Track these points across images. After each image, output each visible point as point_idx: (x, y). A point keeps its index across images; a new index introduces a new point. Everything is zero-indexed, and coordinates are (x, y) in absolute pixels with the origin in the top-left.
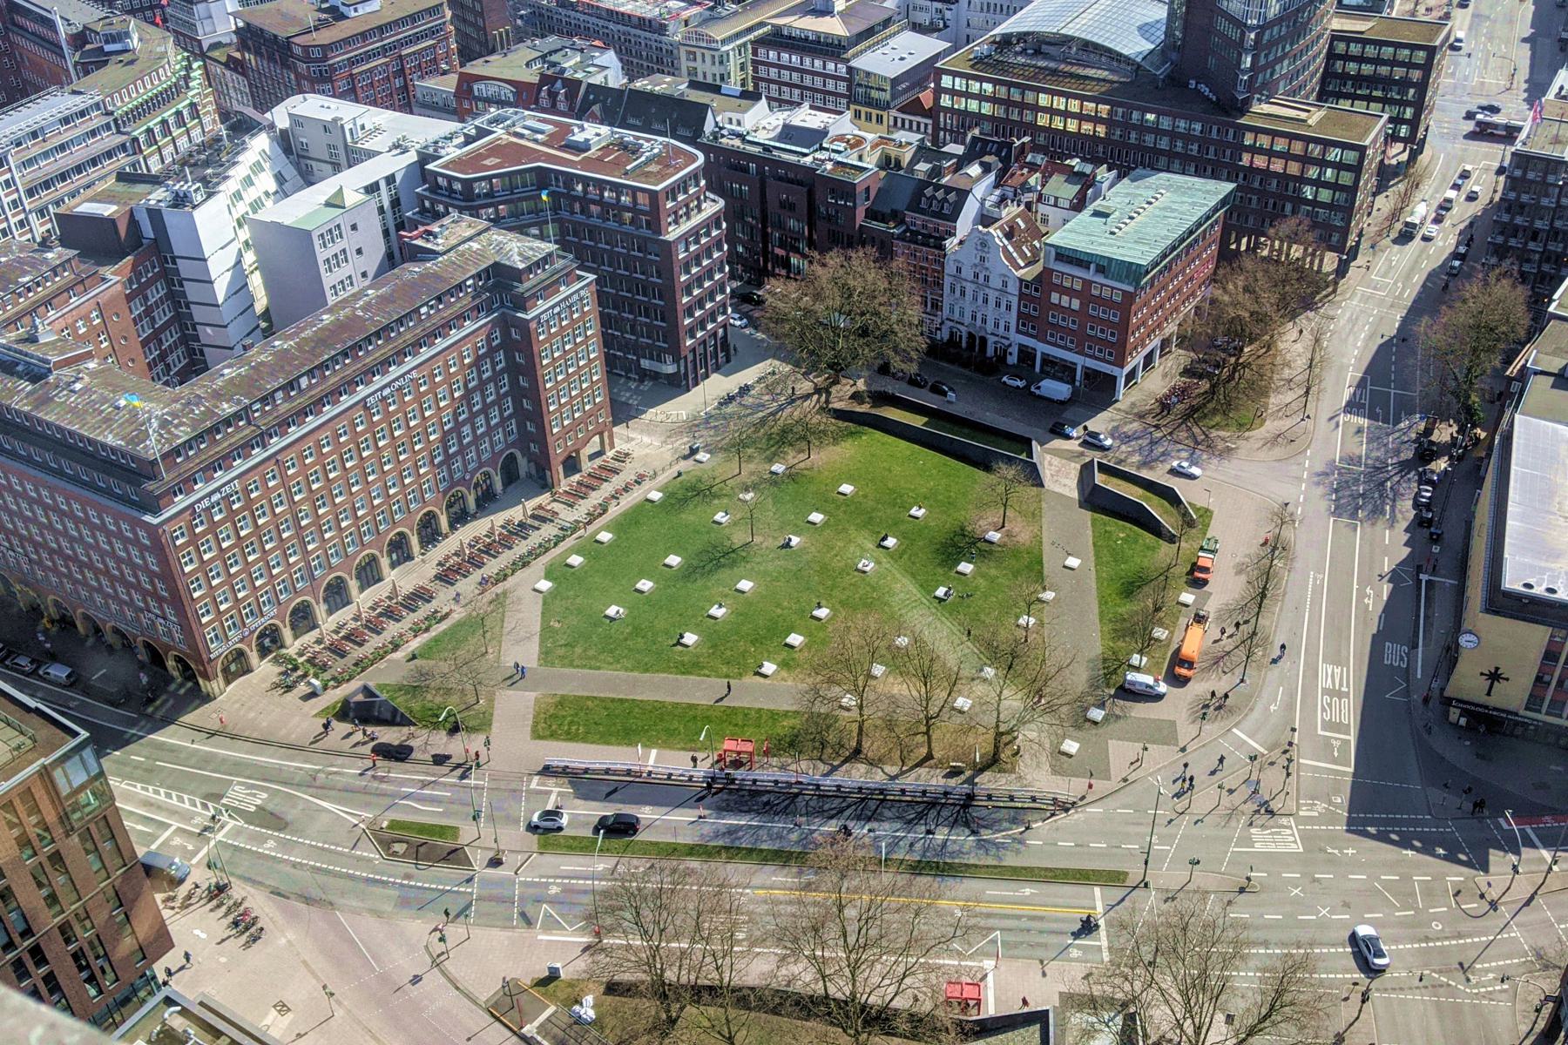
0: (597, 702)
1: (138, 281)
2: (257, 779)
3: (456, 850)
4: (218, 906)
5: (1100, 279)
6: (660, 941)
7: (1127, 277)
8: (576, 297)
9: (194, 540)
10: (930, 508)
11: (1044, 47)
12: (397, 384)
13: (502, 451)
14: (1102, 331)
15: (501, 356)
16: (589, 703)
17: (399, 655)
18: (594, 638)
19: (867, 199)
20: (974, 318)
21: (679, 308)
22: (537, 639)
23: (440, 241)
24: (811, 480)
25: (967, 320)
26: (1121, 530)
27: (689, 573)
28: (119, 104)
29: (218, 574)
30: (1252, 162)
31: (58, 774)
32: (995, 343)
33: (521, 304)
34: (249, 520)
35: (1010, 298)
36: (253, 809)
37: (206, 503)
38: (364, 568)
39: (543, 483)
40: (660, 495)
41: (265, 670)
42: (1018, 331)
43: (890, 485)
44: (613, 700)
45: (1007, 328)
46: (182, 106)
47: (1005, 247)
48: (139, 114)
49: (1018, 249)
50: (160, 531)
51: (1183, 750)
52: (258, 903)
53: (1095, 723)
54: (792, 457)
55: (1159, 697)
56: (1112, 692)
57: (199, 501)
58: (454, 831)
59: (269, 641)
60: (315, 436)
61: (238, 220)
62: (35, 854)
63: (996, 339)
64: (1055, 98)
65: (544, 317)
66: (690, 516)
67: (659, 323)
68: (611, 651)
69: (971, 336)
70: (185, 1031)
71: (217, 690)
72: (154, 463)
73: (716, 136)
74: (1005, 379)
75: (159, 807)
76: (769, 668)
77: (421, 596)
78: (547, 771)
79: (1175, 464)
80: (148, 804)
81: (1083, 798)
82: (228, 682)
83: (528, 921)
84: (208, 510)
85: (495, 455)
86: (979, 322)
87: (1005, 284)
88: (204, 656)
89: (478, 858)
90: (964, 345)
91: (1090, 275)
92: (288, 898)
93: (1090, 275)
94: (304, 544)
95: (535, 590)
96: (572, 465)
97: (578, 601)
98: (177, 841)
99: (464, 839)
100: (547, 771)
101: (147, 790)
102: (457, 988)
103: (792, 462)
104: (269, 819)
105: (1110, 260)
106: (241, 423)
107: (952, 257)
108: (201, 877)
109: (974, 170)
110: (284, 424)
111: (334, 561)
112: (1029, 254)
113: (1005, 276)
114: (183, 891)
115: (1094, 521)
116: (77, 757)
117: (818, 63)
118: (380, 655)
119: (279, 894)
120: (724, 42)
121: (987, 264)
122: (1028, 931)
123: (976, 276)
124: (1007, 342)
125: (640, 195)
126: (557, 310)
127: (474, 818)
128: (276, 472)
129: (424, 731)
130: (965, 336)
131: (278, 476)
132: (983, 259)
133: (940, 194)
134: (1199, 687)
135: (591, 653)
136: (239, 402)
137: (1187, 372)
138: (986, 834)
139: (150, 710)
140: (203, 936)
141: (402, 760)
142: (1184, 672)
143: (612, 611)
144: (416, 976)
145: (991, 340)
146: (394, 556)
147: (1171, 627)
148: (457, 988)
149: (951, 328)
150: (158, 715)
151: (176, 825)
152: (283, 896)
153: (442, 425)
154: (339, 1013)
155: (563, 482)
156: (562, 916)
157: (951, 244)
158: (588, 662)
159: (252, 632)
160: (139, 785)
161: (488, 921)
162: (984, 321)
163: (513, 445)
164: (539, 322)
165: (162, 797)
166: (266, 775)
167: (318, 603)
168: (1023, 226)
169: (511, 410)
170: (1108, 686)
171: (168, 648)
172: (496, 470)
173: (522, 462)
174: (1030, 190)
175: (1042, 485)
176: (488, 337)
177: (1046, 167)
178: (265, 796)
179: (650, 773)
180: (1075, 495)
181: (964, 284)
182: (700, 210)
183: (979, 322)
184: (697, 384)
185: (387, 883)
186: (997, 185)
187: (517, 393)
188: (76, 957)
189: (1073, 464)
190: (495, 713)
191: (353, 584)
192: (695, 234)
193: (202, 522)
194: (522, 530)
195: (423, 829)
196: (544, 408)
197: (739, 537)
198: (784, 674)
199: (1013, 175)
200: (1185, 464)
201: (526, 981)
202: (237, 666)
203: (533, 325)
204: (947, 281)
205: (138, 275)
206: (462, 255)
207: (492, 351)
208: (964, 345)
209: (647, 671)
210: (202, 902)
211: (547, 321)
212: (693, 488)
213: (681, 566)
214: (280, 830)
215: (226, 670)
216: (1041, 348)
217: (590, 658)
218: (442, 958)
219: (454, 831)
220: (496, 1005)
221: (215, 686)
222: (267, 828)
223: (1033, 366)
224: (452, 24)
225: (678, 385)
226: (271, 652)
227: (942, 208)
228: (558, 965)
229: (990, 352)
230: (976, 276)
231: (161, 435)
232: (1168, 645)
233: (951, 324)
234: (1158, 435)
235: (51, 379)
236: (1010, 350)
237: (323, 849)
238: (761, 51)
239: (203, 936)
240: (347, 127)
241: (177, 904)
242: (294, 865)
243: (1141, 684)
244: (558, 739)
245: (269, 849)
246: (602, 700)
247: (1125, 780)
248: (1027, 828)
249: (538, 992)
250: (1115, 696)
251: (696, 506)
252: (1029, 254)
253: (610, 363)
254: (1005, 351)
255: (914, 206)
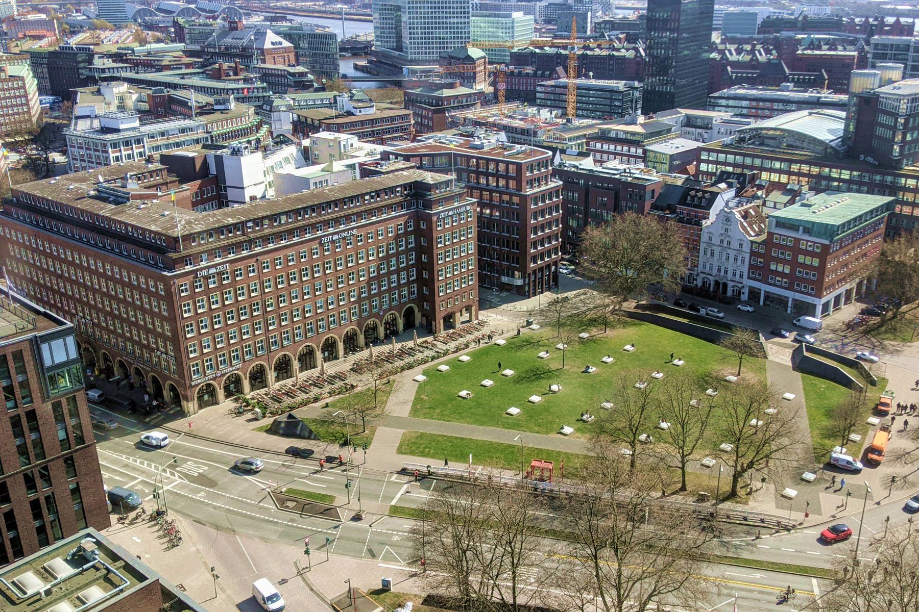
0: (445, 438)
1: (202, 196)
2: (208, 460)
3: (331, 509)
4: (155, 525)
5: (806, 237)
6: (469, 542)
7: (825, 234)
8: (464, 209)
9: (193, 296)
10: (686, 362)
11: (766, 140)
12: (343, 234)
13: (405, 303)
14: (807, 273)
15: (412, 239)
16: (440, 438)
17: (318, 404)
18: (449, 406)
19: (653, 197)
20: (719, 270)
21: (528, 240)
22: (411, 404)
23: (384, 167)
24: (606, 343)
25: (715, 272)
26: (822, 384)
27: (518, 380)
28: (215, 129)
29: (206, 326)
30: (901, 210)
31: (45, 347)
32: (733, 287)
33: (429, 205)
34: (232, 294)
35: (744, 255)
36: (196, 474)
37: (204, 273)
38: (304, 355)
39: (429, 330)
40: (505, 342)
41: (227, 404)
42: (749, 278)
43: (660, 349)
44: (456, 438)
45: (741, 276)
46: (252, 138)
47: (741, 223)
48: (226, 137)
49: (750, 225)
50: (172, 282)
51: (878, 503)
52: (183, 526)
53: (809, 482)
54: (594, 331)
55: (857, 471)
56: (822, 466)
57: (201, 269)
58: (332, 498)
59: (233, 387)
60: (285, 252)
61: (269, 183)
62: (16, 406)
63: (734, 284)
64: (772, 174)
65: (442, 216)
66: (523, 354)
67: (515, 265)
68: (460, 413)
69: (717, 283)
70: (93, 552)
71: (191, 410)
72: (176, 239)
73: (560, 165)
74: (739, 306)
75: (134, 469)
76: (568, 430)
77: (340, 377)
78: (404, 472)
79: (859, 353)
80: (126, 466)
81: (801, 524)
82: (201, 407)
83: (373, 555)
84: (206, 278)
85: (401, 305)
86: (722, 273)
87: (741, 245)
88: (187, 382)
89: (345, 516)
90: (712, 289)
91: (799, 235)
92: (205, 525)
93: (799, 235)
94: (267, 325)
95: (414, 380)
96: (449, 321)
97: (442, 387)
98: (140, 487)
99: (336, 503)
100: (404, 472)
101: (129, 459)
102: (312, 590)
103: (593, 333)
104: (203, 480)
105: (813, 223)
106: (238, 233)
107: (706, 231)
108: (150, 507)
109: (723, 186)
110: (266, 239)
111: (285, 343)
112: (757, 229)
113: (741, 240)
114: (132, 515)
115: (803, 379)
116: (61, 340)
117: (626, 148)
118: (304, 403)
119: (199, 522)
120: (570, 139)
121: (729, 233)
122: (759, 600)
123: (722, 241)
124: (740, 285)
125: (511, 167)
126: (451, 213)
127: (347, 486)
128: (255, 268)
129: (324, 443)
130: (712, 284)
131: (256, 271)
132: (727, 230)
133: (700, 194)
134: (885, 470)
135: (447, 413)
136: (239, 219)
137: (863, 312)
138: (726, 539)
139: (148, 420)
140: (139, 541)
141: (305, 458)
142: (875, 457)
143: (463, 393)
144: (283, 580)
145: (730, 284)
146: (326, 354)
147: (864, 434)
148: (312, 590)
149: (703, 278)
150: (153, 423)
151: (141, 478)
152: (202, 524)
153: (369, 273)
154: (221, 596)
155: (442, 332)
156: (398, 554)
157: (705, 223)
158: (441, 417)
159: (223, 375)
160: (124, 456)
161: (344, 552)
162: (726, 272)
163: (413, 301)
164: (438, 218)
165: (138, 464)
166: (209, 457)
167: (270, 369)
168: (753, 213)
169: (414, 278)
170: (819, 463)
171: (167, 378)
172: (400, 315)
173: (418, 315)
174: (758, 198)
175: (766, 358)
176: (406, 223)
177: (768, 187)
178: (206, 468)
179: (477, 479)
180: (790, 364)
181: (714, 248)
182: (547, 184)
183: (722, 273)
184: (535, 295)
185: (277, 523)
186: (737, 195)
187: (421, 281)
188: (35, 505)
189: (787, 350)
190: (375, 438)
191: (296, 364)
192: (543, 196)
193: (200, 286)
194: (411, 352)
195: (310, 495)
196: (436, 293)
197: (554, 366)
198: (579, 435)
199: (746, 191)
200: (867, 353)
201: (364, 590)
202: (208, 396)
203: (435, 219)
204: (702, 246)
205: (202, 193)
206: (396, 176)
207: (406, 234)
208: (712, 289)
209: (482, 425)
210: (145, 522)
211: (444, 219)
212: (527, 341)
213: (513, 377)
214: (210, 487)
215: (200, 398)
216: (764, 288)
217: (444, 415)
218: (305, 571)
219: (332, 498)
220: (338, 603)
221: (190, 406)
222: (203, 485)
223: (759, 302)
224: (414, 127)
225: (522, 293)
226: (234, 395)
227: (701, 202)
228: (390, 579)
229: (729, 293)
230: (722, 241)
231: (185, 227)
232: (861, 445)
233: (704, 275)
234: (846, 341)
235: (128, 203)
236: (743, 291)
237: (238, 500)
238: (592, 143)
239: (139, 541)
240: (342, 143)
241: (127, 521)
242: (215, 507)
243: (843, 460)
244: (414, 455)
245: (201, 497)
246: (449, 437)
247: (833, 516)
248: (758, 538)
249: (372, 598)
250: (824, 468)
251: (527, 350)
252: (757, 229)
253: (482, 279)
254: (740, 292)
255: (683, 201)
